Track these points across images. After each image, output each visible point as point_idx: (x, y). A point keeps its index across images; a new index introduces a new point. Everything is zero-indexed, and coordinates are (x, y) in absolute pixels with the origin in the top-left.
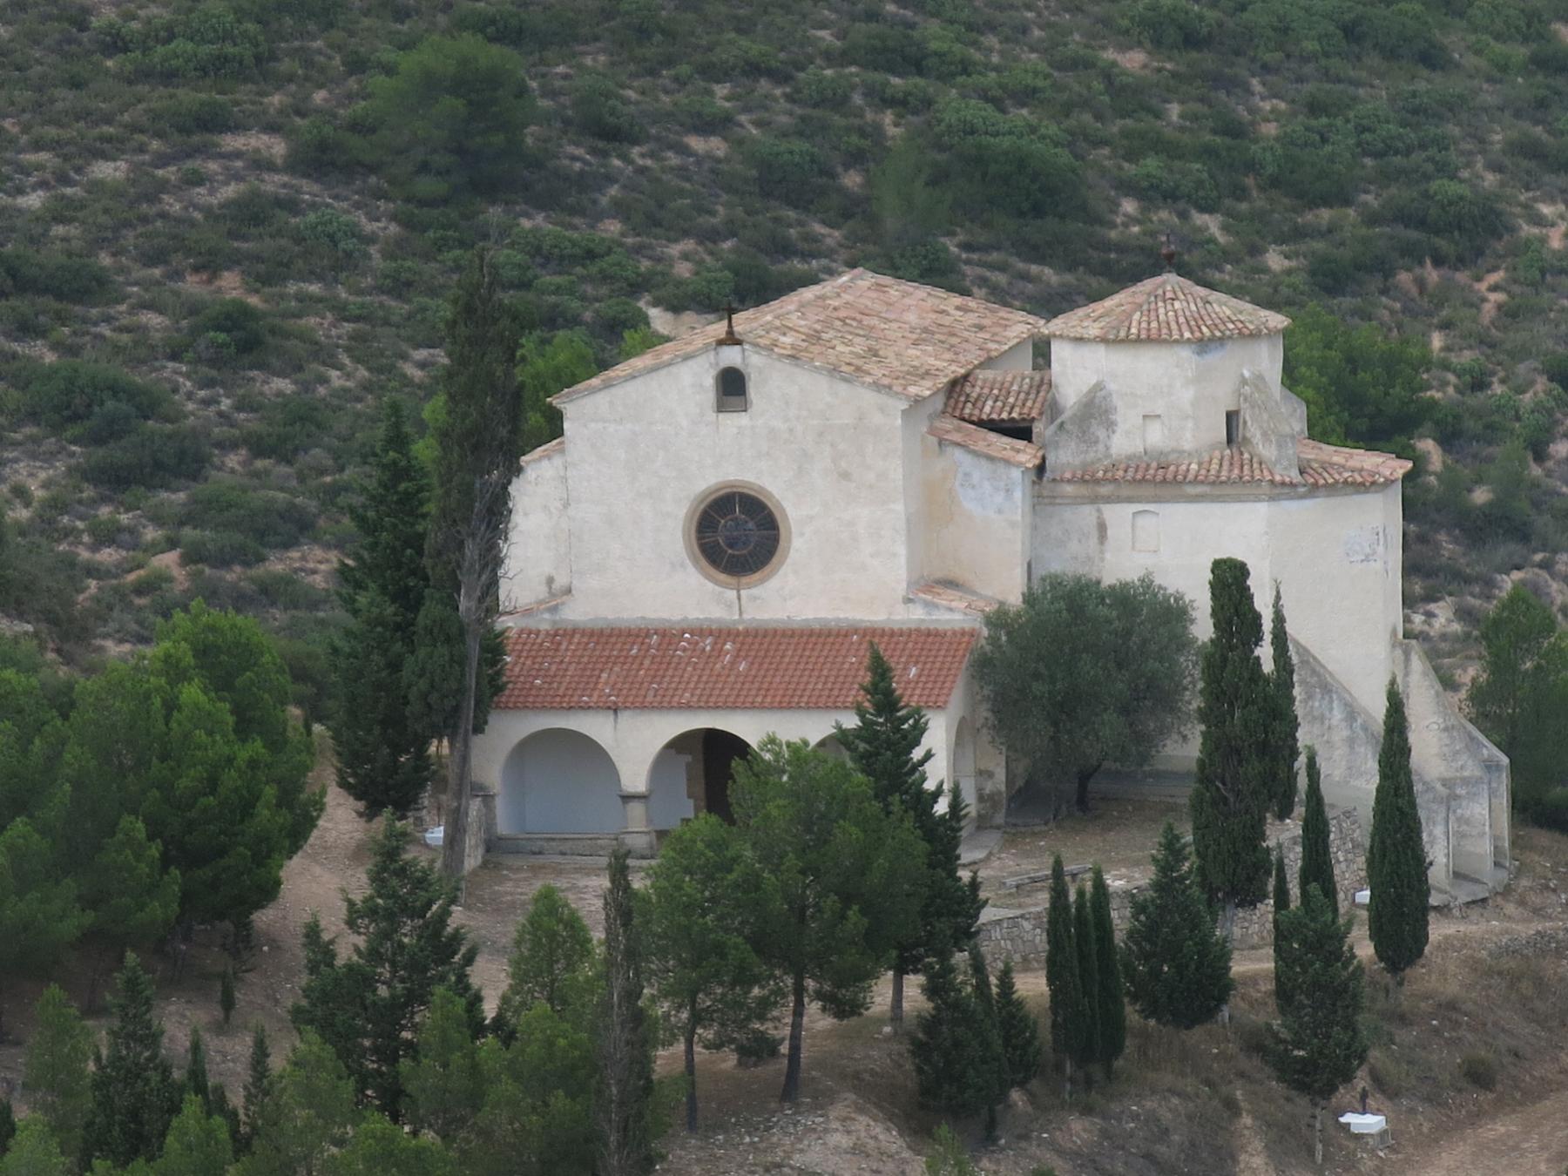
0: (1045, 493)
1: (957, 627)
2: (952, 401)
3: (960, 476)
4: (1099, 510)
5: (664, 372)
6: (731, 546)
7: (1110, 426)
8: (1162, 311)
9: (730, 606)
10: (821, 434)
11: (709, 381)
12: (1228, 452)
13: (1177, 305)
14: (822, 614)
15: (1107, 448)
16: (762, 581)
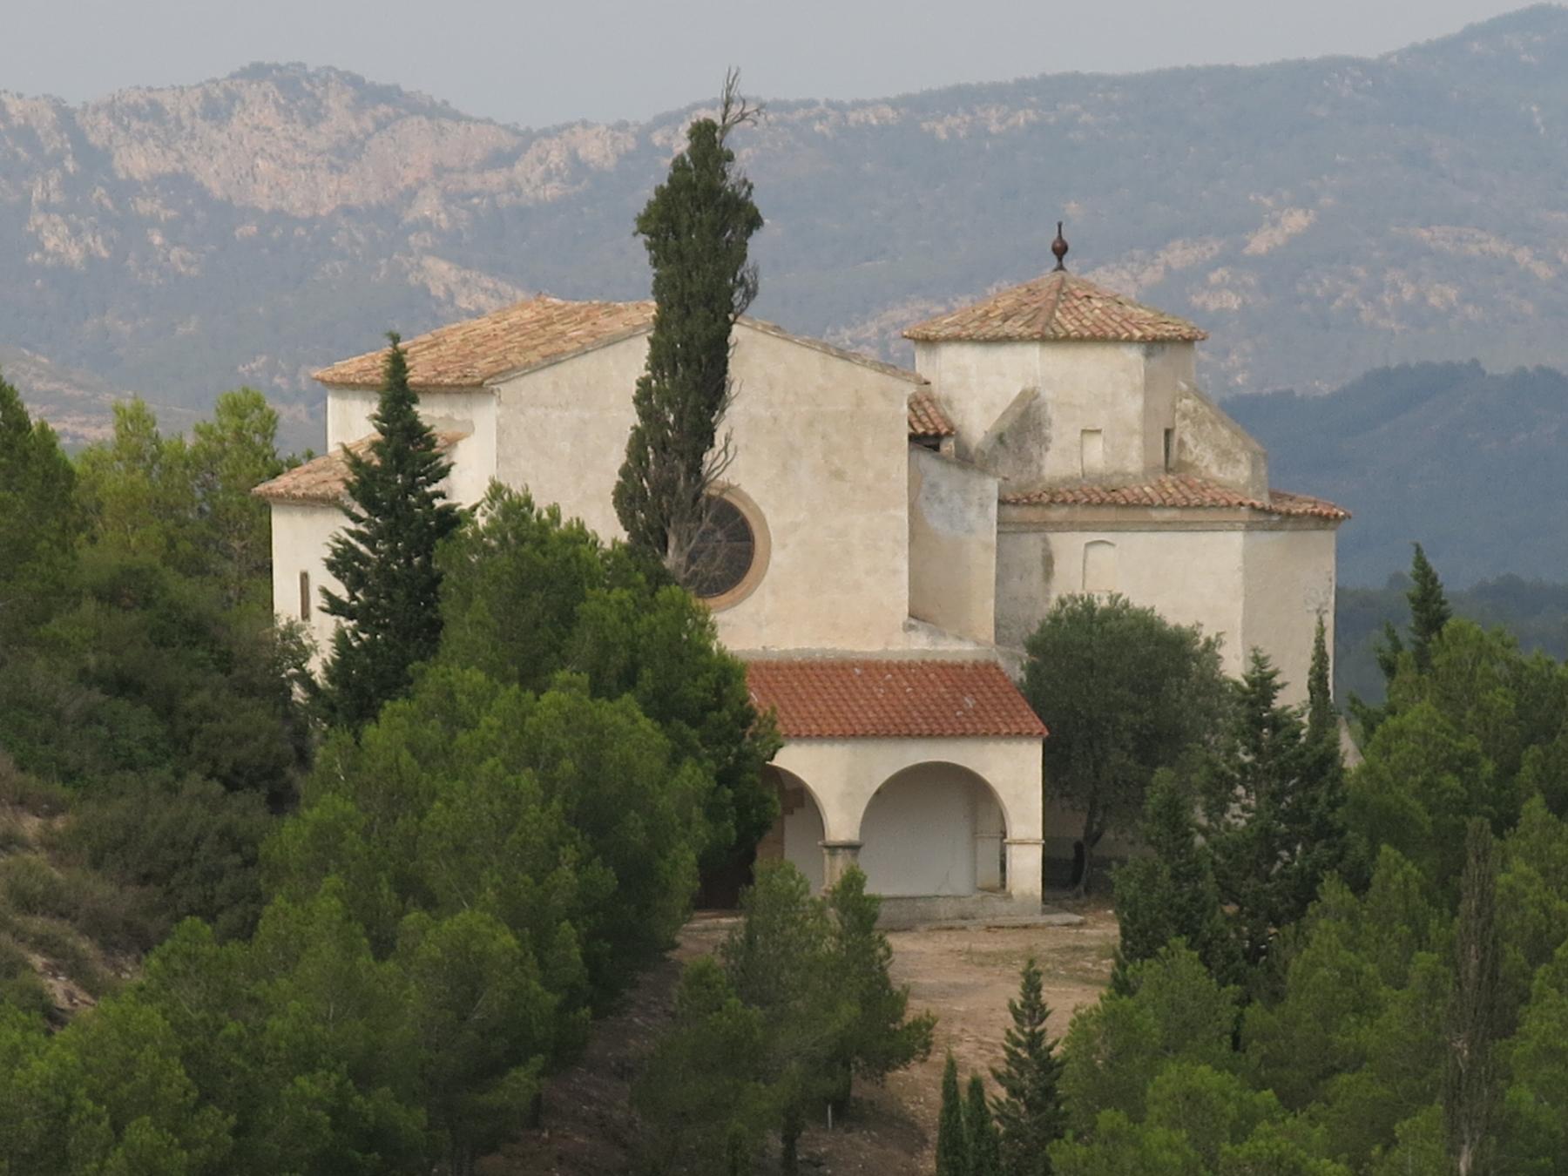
1: (970, 659)
3: (925, 487)
4: (1045, 541)
5: (622, 346)
7: (1044, 442)
10: (811, 424)
14: (806, 645)
15: (1040, 468)
16: (734, 604)
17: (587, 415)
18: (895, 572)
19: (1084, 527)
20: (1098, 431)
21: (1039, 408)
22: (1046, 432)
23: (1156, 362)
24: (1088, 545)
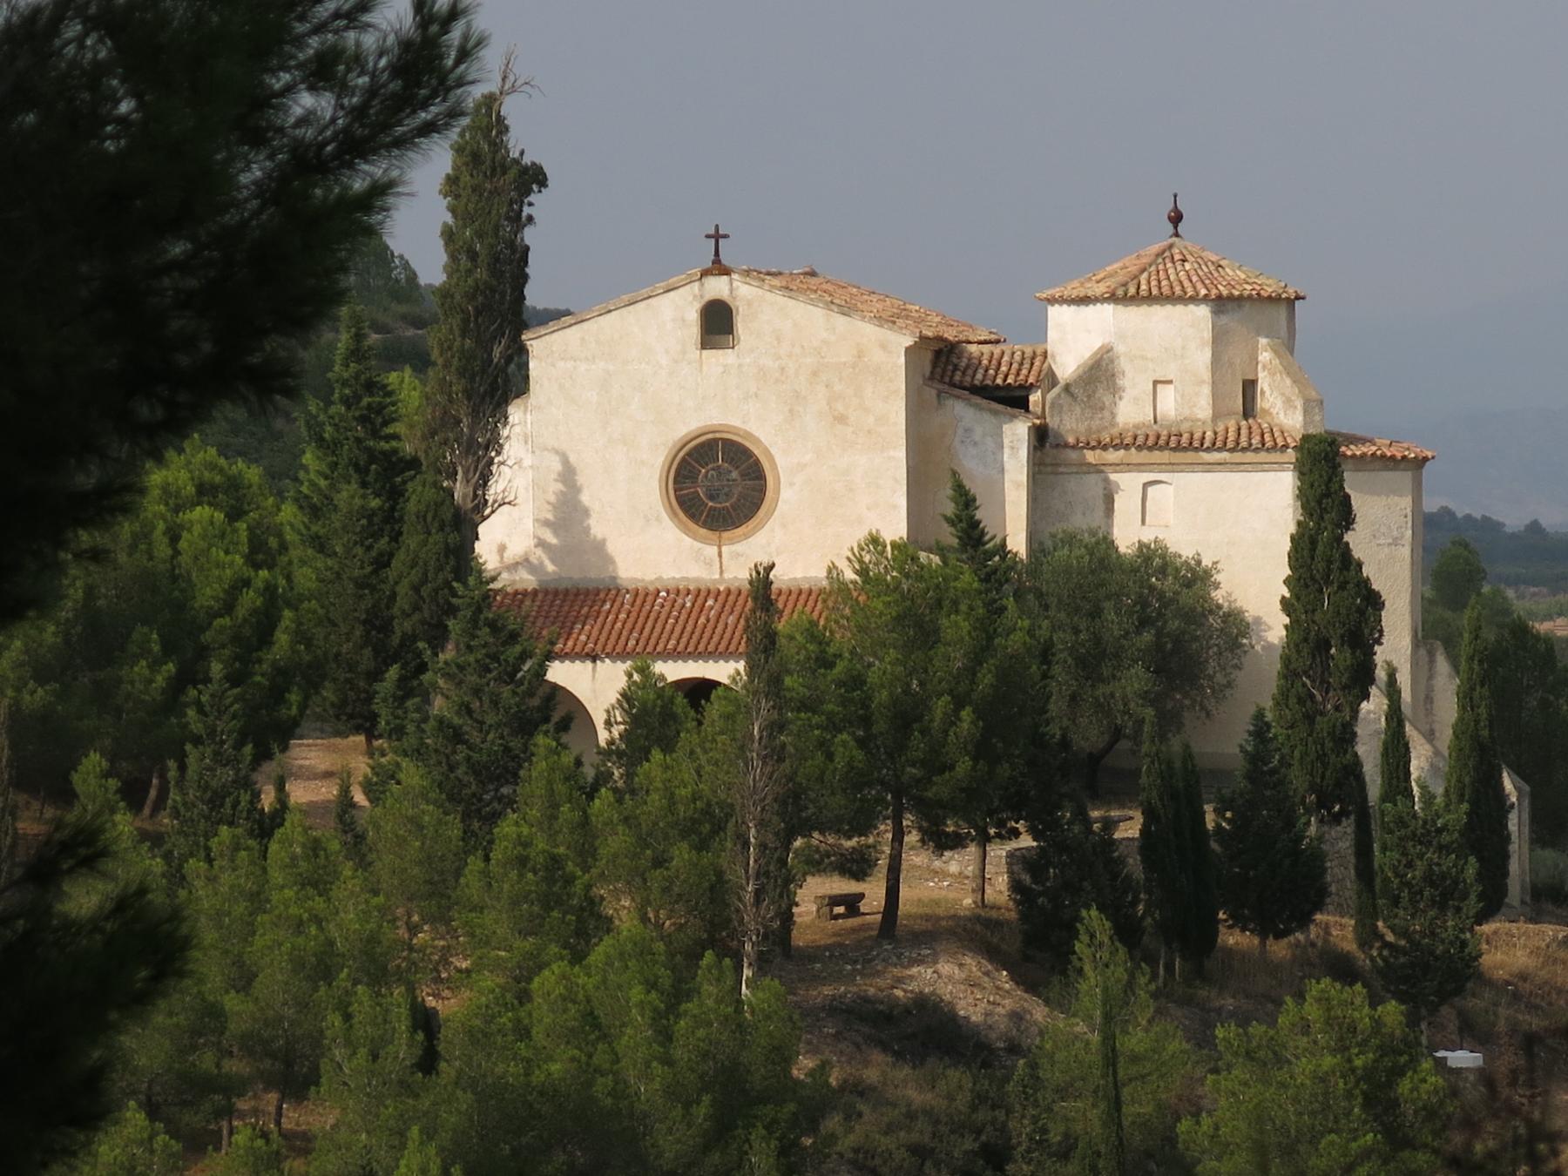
0: (1048, 460)
2: (939, 370)
3: (960, 431)
6: (711, 498)
8: (1171, 271)
9: (709, 564)
11: (693, 316)
12: (1244, 423)
13: (1188, 266)
15: (1113, 415)
16: (747, 536)
17: (611, 368)
18: (895, 507)
19: (1140, 467)
20: (1170, 382)
21: (1112, 361)
22: (1120, 382)
23: (1224, 319)
24: (1146, 485)
